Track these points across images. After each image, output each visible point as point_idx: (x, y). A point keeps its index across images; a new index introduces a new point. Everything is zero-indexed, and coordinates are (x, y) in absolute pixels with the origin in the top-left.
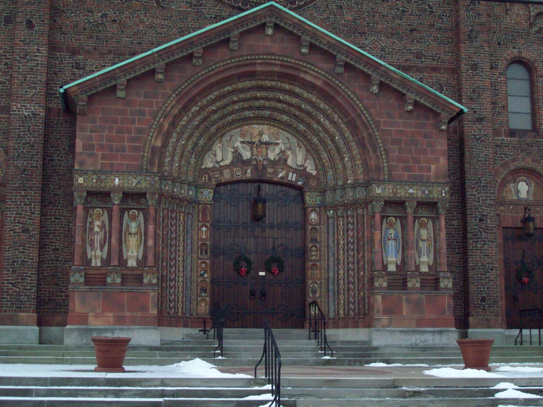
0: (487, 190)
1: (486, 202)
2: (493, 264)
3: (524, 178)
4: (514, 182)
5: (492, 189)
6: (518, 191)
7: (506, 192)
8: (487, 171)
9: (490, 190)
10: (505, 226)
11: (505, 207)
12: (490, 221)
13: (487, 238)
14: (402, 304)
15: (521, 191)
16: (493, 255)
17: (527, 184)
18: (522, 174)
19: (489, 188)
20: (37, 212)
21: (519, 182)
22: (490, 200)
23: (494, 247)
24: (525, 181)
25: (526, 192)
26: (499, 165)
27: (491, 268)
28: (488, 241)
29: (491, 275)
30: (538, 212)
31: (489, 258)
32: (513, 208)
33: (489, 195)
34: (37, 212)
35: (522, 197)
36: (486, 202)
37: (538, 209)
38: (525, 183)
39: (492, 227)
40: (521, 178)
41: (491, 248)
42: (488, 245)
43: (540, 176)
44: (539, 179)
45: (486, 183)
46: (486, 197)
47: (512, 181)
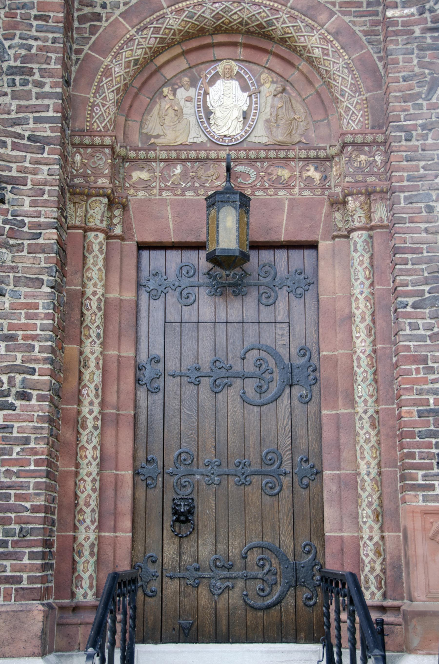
0: (25, 83)
1: (18, 129)
2: (33, 372)
3: (235, 67)
4: (193, 83)
5: (47, 80)
6: (209, 113)
7: (162, 119)
8: (34, 12)
9: (41, 85)
10: (150, 238)
11: (151, 170)
12: (33, 204)
13: (14, 269)
14: (70, 470)
15: (218, 113)
16: (34, 337)
17: (244, 88)
18: (218, 52)
19: (37, 77)
20: (37, 366)
21: (212, 82)
22: (37, 120)
23: (41, 302)
24: (239, 77)
25: (237, 113)
26: (117, 12)
27: (18, 388)
28: (17, 282)
29: (18, 419)
30: (287, 186)
31: (18, 348)
32: (184, 175)
33: (33, 102)
34: (37, 366)
35: (223, 131)
36: (18, 129)
37: (285, 173)
38: (235, 85)
39: (39, 225)
40: (221, 67)
41: (27, 306)
42: (15, 295)
43: (294, 49)
44: (292, 65)
45: (25, 59)
46: (20, 109)
47: (186, 79)
